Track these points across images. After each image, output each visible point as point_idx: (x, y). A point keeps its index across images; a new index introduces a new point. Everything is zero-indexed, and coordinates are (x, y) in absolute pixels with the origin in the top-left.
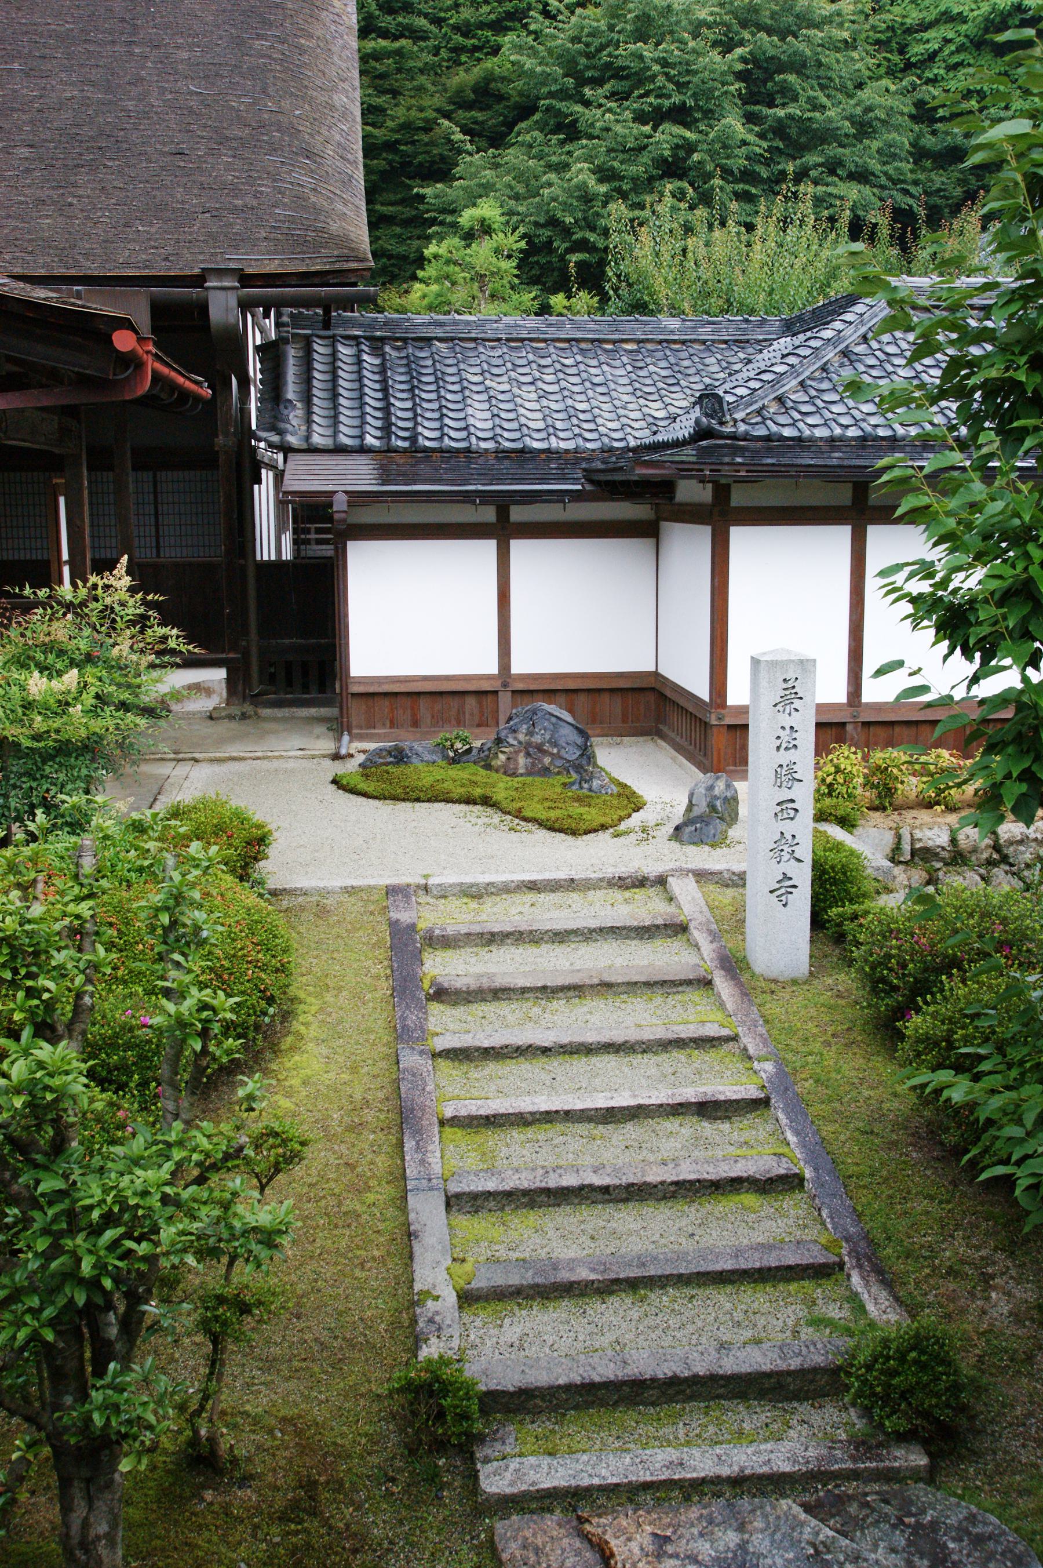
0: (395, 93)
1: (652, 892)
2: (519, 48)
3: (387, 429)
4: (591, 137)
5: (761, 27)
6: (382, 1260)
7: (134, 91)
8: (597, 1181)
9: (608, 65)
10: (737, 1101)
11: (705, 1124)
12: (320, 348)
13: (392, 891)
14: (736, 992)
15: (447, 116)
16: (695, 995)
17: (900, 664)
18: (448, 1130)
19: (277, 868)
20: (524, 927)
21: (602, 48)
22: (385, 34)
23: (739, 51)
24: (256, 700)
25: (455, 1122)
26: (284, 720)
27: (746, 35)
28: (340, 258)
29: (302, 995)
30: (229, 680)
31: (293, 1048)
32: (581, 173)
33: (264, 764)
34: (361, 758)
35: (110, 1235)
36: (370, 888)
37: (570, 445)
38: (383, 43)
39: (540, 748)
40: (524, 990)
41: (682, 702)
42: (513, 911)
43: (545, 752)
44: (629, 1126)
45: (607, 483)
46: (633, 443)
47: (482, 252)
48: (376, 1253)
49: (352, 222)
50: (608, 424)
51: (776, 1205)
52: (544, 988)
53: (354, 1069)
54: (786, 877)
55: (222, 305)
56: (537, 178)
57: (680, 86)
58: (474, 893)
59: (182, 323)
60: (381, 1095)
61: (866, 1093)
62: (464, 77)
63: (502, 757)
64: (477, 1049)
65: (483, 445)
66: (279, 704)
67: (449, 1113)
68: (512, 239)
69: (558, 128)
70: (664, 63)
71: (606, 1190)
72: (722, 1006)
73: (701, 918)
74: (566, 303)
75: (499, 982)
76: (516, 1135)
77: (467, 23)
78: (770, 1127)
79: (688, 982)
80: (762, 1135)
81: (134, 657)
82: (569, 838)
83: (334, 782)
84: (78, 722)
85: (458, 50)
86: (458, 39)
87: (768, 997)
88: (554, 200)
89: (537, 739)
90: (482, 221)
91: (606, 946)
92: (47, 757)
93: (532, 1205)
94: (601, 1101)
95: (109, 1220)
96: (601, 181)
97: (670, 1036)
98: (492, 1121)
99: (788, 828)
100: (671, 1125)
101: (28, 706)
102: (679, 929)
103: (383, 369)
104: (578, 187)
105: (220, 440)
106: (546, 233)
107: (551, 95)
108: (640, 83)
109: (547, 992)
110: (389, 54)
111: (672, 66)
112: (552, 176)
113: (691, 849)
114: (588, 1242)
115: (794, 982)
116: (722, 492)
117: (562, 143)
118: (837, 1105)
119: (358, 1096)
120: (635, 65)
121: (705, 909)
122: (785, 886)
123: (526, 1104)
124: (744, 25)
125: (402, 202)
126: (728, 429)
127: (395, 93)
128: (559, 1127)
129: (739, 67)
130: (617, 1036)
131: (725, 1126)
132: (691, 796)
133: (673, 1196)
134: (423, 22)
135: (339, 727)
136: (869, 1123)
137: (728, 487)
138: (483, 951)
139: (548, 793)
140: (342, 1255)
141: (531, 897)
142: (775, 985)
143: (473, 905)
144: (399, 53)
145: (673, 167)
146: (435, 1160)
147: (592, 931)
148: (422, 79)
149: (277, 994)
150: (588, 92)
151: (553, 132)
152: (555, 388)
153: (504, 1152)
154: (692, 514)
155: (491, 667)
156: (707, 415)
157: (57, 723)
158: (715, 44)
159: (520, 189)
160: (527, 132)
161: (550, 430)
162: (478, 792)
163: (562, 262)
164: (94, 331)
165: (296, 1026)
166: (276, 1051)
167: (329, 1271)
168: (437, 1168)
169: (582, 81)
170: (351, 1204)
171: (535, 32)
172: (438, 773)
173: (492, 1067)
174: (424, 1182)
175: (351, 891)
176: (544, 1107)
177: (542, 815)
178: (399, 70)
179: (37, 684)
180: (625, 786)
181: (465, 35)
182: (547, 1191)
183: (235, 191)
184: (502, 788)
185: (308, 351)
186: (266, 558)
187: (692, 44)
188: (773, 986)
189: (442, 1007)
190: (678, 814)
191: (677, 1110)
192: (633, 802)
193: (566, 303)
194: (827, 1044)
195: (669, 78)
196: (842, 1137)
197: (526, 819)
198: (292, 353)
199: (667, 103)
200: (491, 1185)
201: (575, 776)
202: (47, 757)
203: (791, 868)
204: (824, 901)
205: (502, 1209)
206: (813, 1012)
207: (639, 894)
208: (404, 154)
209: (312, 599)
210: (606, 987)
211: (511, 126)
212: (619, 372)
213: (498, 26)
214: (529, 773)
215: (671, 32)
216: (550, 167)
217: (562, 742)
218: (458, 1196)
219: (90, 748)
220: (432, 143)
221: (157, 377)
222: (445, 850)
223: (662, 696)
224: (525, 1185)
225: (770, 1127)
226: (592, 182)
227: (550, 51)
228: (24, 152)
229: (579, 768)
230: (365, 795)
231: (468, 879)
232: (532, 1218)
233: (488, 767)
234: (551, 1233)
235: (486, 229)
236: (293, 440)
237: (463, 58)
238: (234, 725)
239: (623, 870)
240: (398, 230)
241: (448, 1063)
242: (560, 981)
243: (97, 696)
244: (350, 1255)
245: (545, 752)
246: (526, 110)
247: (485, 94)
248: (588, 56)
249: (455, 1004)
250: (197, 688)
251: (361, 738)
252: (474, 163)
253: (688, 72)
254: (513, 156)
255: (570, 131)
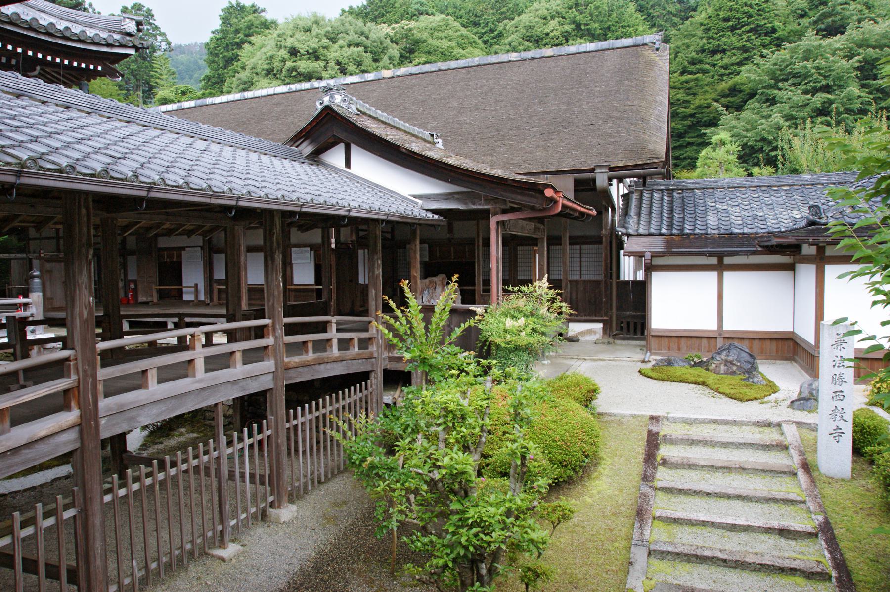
0: (694, 95)
1: (774, 430)
2: (749, 71)
3: (671, 226)
4: (782, 103)
5: (868, 46)
6: (616, 572)
7: (578, 104)
8: (721, 556)
9: (790, 73)
10: (800, 532)
11: (782, 540)
12: (646, 195)
13: (652, 418)
14: (809, 480)
15: (717, 101)
16: (788, 479)
17: (846, 319)
18: (656, 521)
19: (601, 403)
20: (708, 439)
21: (787, 66)
22: (691, 73)
23: (857, 58)
24: (614, 337)
25: (660, 518)
26: (626, 345)
27: (861, 51)
28: (650, 158)
29: (605, 456)
30: (603, 328)
31: (597, 478)
32: (777, 118)
33: (613, 363)
34: (654, 363)
35: (474, 530)
36: (643, 416)
37: (753, 231)
38: (690, 76)
39: (731, 363)
40: (703, 466)
41: (804, 346)
42: (705, 431)
43: (734, 364)
44: (743, 534)
45: (767, 246)
46: (783, 230)
47: (721, 153)
48: (614, 568)
49: (658, 144)
50: (771, 222)
51: (815, 586)
52: (713, 466)
53: (621, 490)
54: (838, 428)
55: (601, 180)
56: (756, 122)
57: (825, 77)
58: (689, 422)
59: (585, 187)
60: (630, 502)
61: (877, 541)
62: (724, 86)
63: (714, 365)
64: (676, 489)
65: (713, 232)
66: (624, 339)
67: (657, 515)
68: (734, 147)
69: (767, 100)
70: (818, 68)
71: (725, 561)
72: (800, 486)
73: (796, 444)
74: (759, 171)
75: (692, 461)
76: (688, 529)
77: (727, 65)
78: (817, 548)
79: (785, 473)
80: (812, 550)
81: (549, 314)
82: (739, 403)
83: (639, 371)
84: (524, 339)
85: (722, 75)
86: (723, 71)
87: (827, 485)
88: (764, 130)
89: (730, 358)
90: (721, 140)
91: (746, 452)
92: (510, 351)
93: (689, 561)
94: (730, 521)
95: (475, 524)
96: (786, 120)
97: (770, 496)
98: (676, 521)
99: (840, 405)
100: (764, 537)
101: (506, 331)
102: (783, 447)
103: (671, 202)
104: (776, 124)
105: (604, 232)
106: (760, 144)
107: (763, 88)
108: (805, 78)
109: (714, 468)
110: (692, 80)
111: (822, 69)
112: (763, 121)
113: (798, 412)
114: (712, 583)
115: (843, 480)
116: (821, 250)
117: (769, 106)
118: (858, 544)
119: (620, 502)
120: (803, 71)
121: (799, 440)
122: (837, 433)
123: (694, 516)
124: (860, 47)
125: (697, 136)
126: (823, 221)
127: (694, 95)
128: (709, 529)
129: (857, 65)
130: (744, 492)
131: (793, 543)
132: (801, 388)
133: (759, 570)
134: (707, 67)
135: (648, 348)
136: (876, 556)
137: (824, 247)
138: (688, 448)
139: (733, 382)
140: (600, 566)
141: (714, 426)
142: (831, 480)
143: (687, 427)
144: (696, 79)
145: (823, 111)
146: (647, 533)
147: (740, 444)
148: (706, 88)
149: (591, 454)
150: (780, 85)
151: (764, 103)
152: (748, 207)
153: (680, 535)
154: (807, 260)
155: (714, 326)
156: (813, 215)
157: (514, 338)
158: (844, 57)
159: (749, 127)
160: (752, 104)
161: (745, 224)
162: (700, 380)
163: (754, 154)
164: (537, 189)
165: (600, 469)
166: (589, 478)
167: (592, 572)
168: (647, 537)
169: (777, 80)
170: (608, 546)
171: (757, 64)
172: (684, 370)
173: (682, 498)
174: (640, 542)
175: (634, 416)
176: (702, 519)
177: (727, 391)
178: (696, 86)
179: (509, 323)
180: (770, 382)
181: (725, 69)
182: (696, 556)
183: (611, 136)
184: (711, 378)
185: (641, 196)
186: (627, 279)
187: (831, 59)
188: (830, 481)
189: (664, 469)
190: (795, 396)
191: (768, 530)
192: (774, 389)
193: (759, 171)
194: (857, 513)
195: (820, 74)
196: (858, 560)
197: (720, 393)
198: (635, 197)
199: (819, 85)
200: (670, 549)
201: (747, 375)
202: (510, 351)
203: (841, 424)
204: (864, 442)
205: (675, 560)
206: (851, 496)
207: (767, 430)
208: (698, 118)
209: (637, 295)
210: (742, 470)
211: (745, 102)
212: (782, 197)
213: (740, 64)
214: (726, 373)
215: (822, 55)
216: (763, 117)
217: (742, 360)
218: (654, 551)
219: (527, 349)
220: (710, 112)
221: (564, 206)
222: (683, 404)
223: (796, 343)
224: (686, 551)
225: (817, 548)
226: (781, 121)
227: (763, 70)
228: (535, 130)
229: (749, 372)
230: (651, 378)
231: (686, 416)
232: (688, 567)
233: (707, 369)
234: (695, 576)
235: (723, 143)
236: (631, 231)
237: (725, 78)
238: (604, 346)
239: (760, 418)
240: (695, 148)
241: (663, 493)
242: (720, 465)
243: (533, 329)
244: (482, 524)
245: (734, 364)
246: (752, 95)
247: (734, 91)
248: (781, 70)
249: (671, 469)
250: (590, 332)
251: (655, 354)
252: (727, 118)
253: (830, 71)
254: (746, 114)
255: (772, 101)
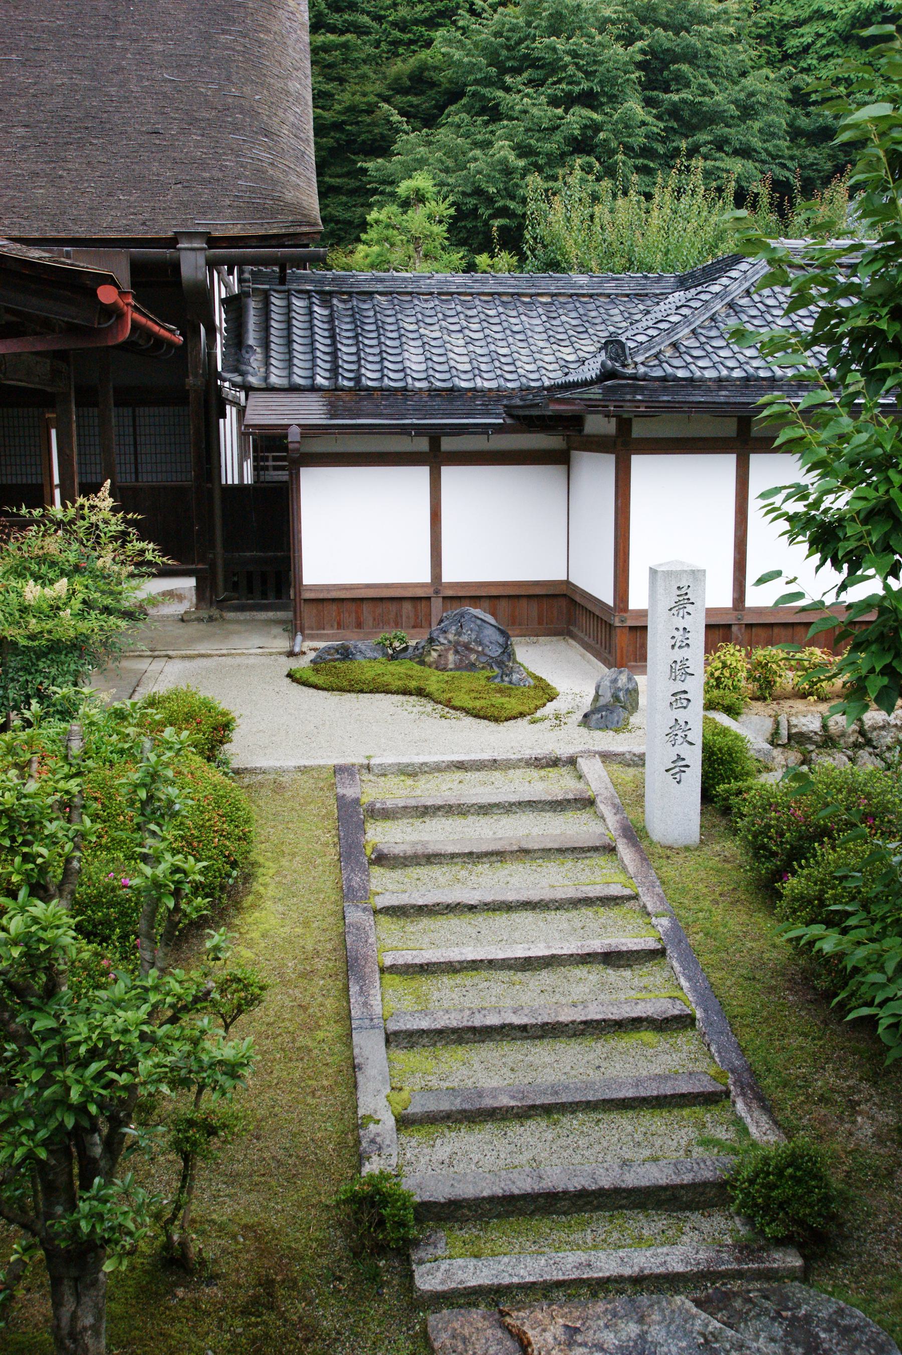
0: (342, 80)
1: (564, 770)
2: (449, 42)
3: (334, 371)
4: (511, 119)
5: (658, 24)
6: (330, 1089)
7: (116, 79)
8: (517, 1020)
9: (526, 57)
10: (637, 952)
11: (610, 971)
12: (277, 301)
13: (339, 770)
14: (637, 857)
15: (387, 100)
16: (601, 860)
17: (779, 574)
18: (387, 976)
19: (240, 750)
20: (453, 801)
21: (520, 41)
22: (333, 30)
23: (639, 44)
24: (221, 605)
25: (393, 969)
26: (246, 622)
27: (645, 30)
28: (294, 223)
29: (261, 860)
30: (198, 588)
31: (253, 906)
32: (503, 149)
33: (228, 661)
34: (312, 655)
35: (95, 1067)
36: (320, 768)
37: (493, 385)
38: (331, 37)
39: (467, 647)
40: (453, 856)
41: (589, 606)
42: (444, 787)
43: (471, 650)
44: (544, 973)
45: (525, 417)
46: (547, 383)
47: (417, 218)
48: (325, 1083)
49: (304, 192)
50: (526, 367)
51: (672, 1041)
52: (471, 854)
53: (306, 924)
54: (680, 758)
55: (192, 263)
56: (464, 154)
57: (588, 75)
58: (410, 772)
59: (158, 279)
60: (329, 946)
61: (749, 945)
62: (401, 67)
63: (434, 654)
64: (413, 906)
65: (418, 385)
66: (241, 608)
67: (388, 962)
68: (443, 206)
69: (483, 111)
70: (574, 54)
71: (524, 1028)
72: (624, 869)
73: (606, 794)
74: (489, 262)
75: (432, 849)
76: (446, 980)
77: (404, 20)
78: (666, 974)
79: (595, 849)
80: (659, 981)
81: (116, 568)
82: (492, 725)
83: (289, 675)
84: (68, 624)
85: (396, 43)
86: (396, 33)
87: (664, 862)
88: (479, 173)
89: (464, 638)
90: (417, 191)
91: (524, 818)
92: (41, 654)
93: (460, 1041)
94: (520, 952)
95: (94, 1054)
96: (519, 156)
97: (580, 895)
98: (425, 969)
99: (682, 715)
100: (580, 972)
101: (24, 610)
102: (587, 803)
103: (331, 319)
104: (500, 162)
105: (190, 380)
106: (472, 201)
107: (477, 82)
108: (553, 72)
109: (473, 857)
110: (337, 47)
111: (581, 57)
112: (478, 152)
113: (598, 734)
114: (509, 1073)
115: (687, 848)
116: (624, 425)
117: (486, 124)
118: (724, 955)
119: (309, 947)
120: (549, 56)
121: (610, 785)
122: (679, 766)
123: (455, 954)
124: (643, 21)
125: (348, 174)
126: (630, 371)
127: (342, 80)
128: (484, 974)
129: (639, 58)
130: (534, 895)
131: (627, 973)
132: (598, 688)
133: (582, 1033)
134: (366, 19)
135: (293, 628)
136: (752, 971)
137: (630, 420)
138: (417, 822)
139: (474, 686)
140: (296, 1085)
141: (459, 775)
142: (670, 851)
143: (409, 782)
144: (345, 45)
145: (582, 145)
146: (376, 1002)
147: (512, 804)
148: (365, 69)
149: (239, 859)
150: (508, 79)
151: (478, 114)
152: (480, 335)
153: (436, 995)
154: (598, 445)
155: (425, 577)
156: (611, 359)
157: (49, 625)
158: (619, 38)
159: (450, 163)
160: (456, 114)
161: (475, 372)
162: (413, 684)
163: (486, 227)
164: (81, 286)
165: (256, 886)
166: (239, 908)
167: (284, 1099)
168: (378, 1009)
169: (504, 70)
170: (303, 1040)
171: (463, 28)
172: (379, 668)
173: (425, 922)
174: (367, 1021)
175: (303, 770)
176: (470, 957)
177: (469, 704)
178: (345, 61)
179: (32, 591)
180: (540, 679)
181: (402, 30)
182: (473, 1029)
183: (203, 165)
184: (434, 681)
185: (267, 303)
186: (230, 482)
187: (598, 38)
188: (668, 852)
189: (382, 870)
190: (586, 704)
191: (586, 959)
192: (548, 693)
193: (489, 262)
194: (715, 902)
195: (579, 67)
196: (728, 983)
197: (455, 708)
198: (253, 305)
199: (577, 89)
200: (425, 1024)
201: (497, 671)
202: (41, 654)
203: (684, 750)
204: (713, 779)
205: (434, 1045)
206: (703, 874)
207: (553, 772)
208: (349, 133)
209: (270, 518)
210: (524, 853)
211: (442, 109)
212: (535, 321)
213: (431, 23)
214: (458, 668)
215: (581, 28)
216: (476, 144)
217: (486, 641)
218: (396, 1033)
219: (77, 647)
220: (374, 124)
221: (136, 326)
222: (385, 734)
223: (573, 602)
224: (454, 1024)
225: (666, 974)
226: (512, 157)
227: (476, 44)
228: (21, 131)
229: (500, 664)
230: (316, 687)
231: (405, 760)
232: (460, 1052)
233: (422, 663)
234: (476, 1066)
235: (420, 198)
236: (253, 380)
237: (401, 50)
238: (202, 626)
239: (539, 751)
240: (344, 199)
241: (388, 918)
242: (484, 848)
243: (84, 602)
245: (471, 650)
246: (455, 95)
247: (420, 81)
248: (509, 48)
249: (393, 868)
250: (170, 594)
251: (312, 637)
252: (410, 141)
253: (595, 62)
254: (443, 135)
255: (493, 113)
